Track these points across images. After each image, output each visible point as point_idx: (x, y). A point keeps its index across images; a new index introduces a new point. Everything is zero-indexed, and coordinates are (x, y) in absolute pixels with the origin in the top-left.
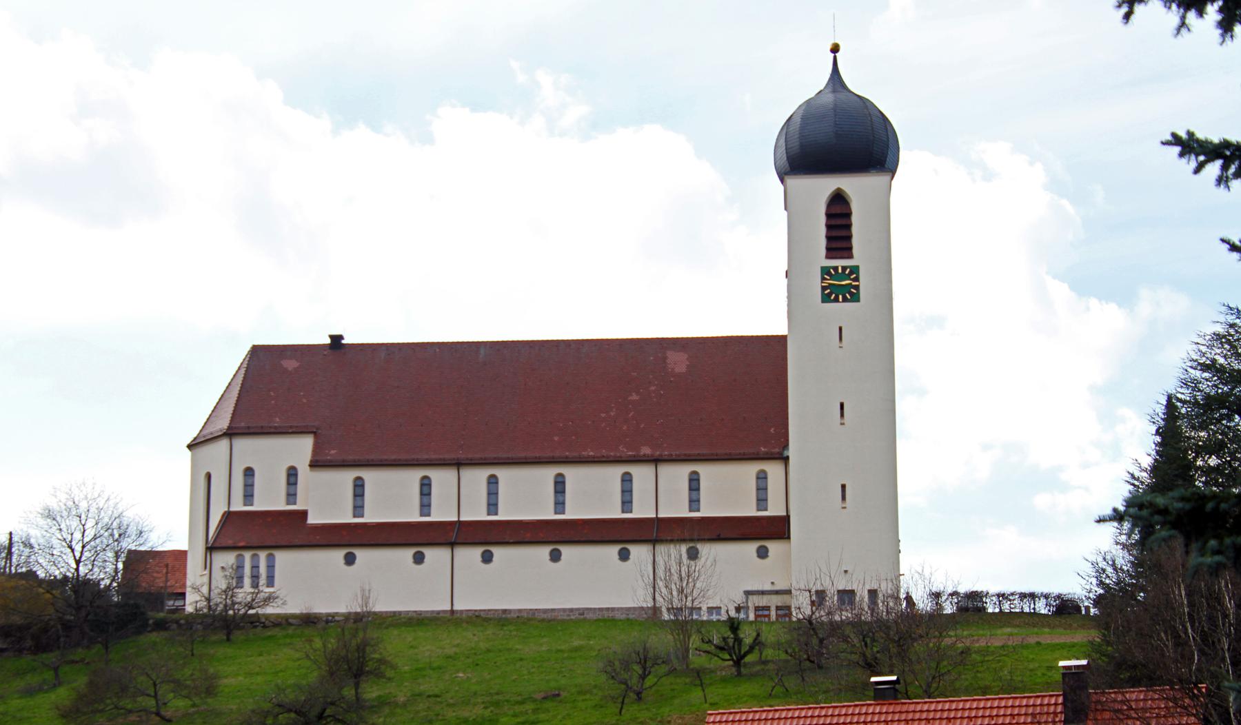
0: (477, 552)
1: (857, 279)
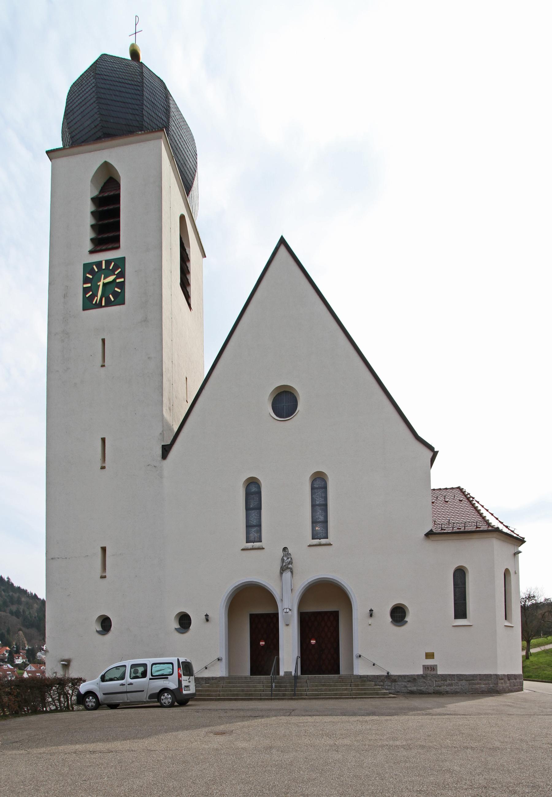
0: (356, 662)
1: (122, 275)
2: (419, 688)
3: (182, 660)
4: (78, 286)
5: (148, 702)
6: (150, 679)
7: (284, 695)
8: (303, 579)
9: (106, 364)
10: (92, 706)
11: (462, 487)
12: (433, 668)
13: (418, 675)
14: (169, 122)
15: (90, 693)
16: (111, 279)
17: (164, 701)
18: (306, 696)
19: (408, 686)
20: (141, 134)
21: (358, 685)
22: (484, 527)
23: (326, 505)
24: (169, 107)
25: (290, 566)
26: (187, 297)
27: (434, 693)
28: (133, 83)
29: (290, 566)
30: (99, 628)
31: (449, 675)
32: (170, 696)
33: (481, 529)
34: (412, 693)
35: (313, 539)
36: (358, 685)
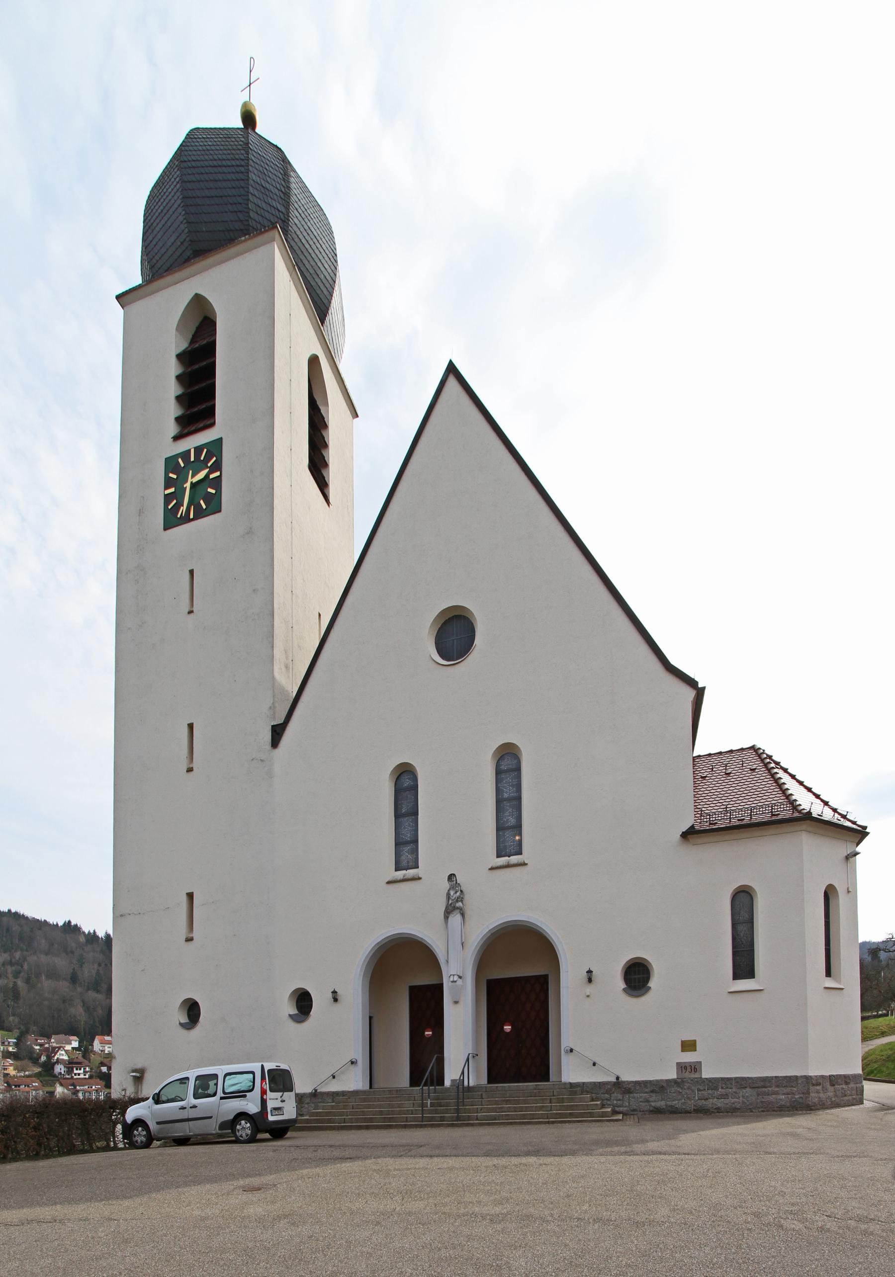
1: (217, 466)
2: (670, 1103)
3: (269, 1066)
4: (159, 492)
5: (220, 1136)
6: (222, 1098)
7: (442, 1119)
8: (481, 924)
9: (195, 609)
10: (142, 1142)
11: (758, 746)
12: (695, 1067)
13: (668, 1081)
14: (288, 213)
15: (139, 1122)
16: (201, 475)
17: (240, 1133)
18: (477, 1119)
19: (651, 1099)
20: (246, 240)
21: (562, 1100)
22: (787, 814)
23: (519, 798)
24: (289, 188)
25: (459, 904)
26: (322, 484)
27: (694, 1110)
28: (233, 163)
29: (459, 904)
30: (294, 1011)
31: (722, 1079)
32: (248, 1125)
33: (779, 817)
34: (657, 1112)
35: (498, 857)
36: (562, 1100)
